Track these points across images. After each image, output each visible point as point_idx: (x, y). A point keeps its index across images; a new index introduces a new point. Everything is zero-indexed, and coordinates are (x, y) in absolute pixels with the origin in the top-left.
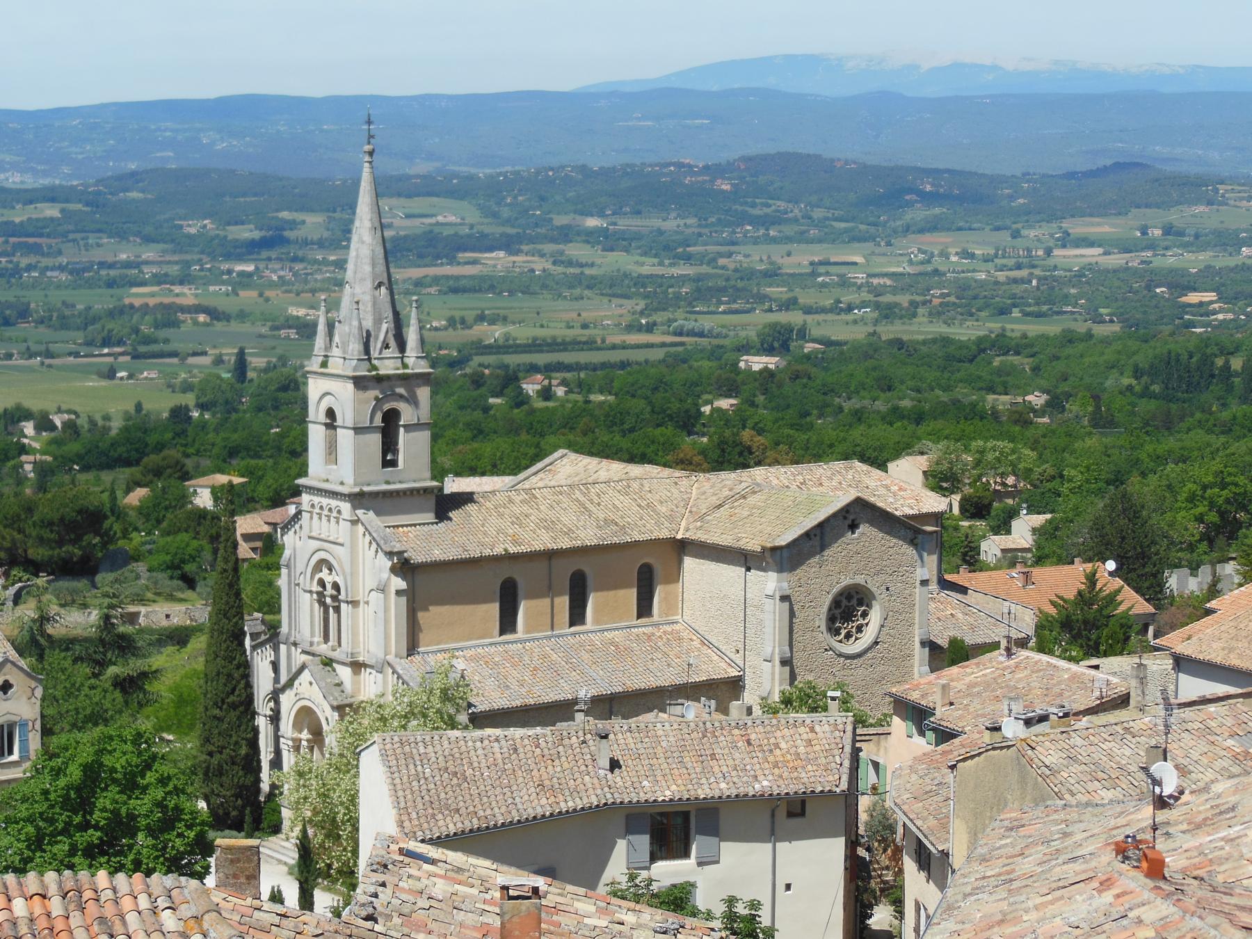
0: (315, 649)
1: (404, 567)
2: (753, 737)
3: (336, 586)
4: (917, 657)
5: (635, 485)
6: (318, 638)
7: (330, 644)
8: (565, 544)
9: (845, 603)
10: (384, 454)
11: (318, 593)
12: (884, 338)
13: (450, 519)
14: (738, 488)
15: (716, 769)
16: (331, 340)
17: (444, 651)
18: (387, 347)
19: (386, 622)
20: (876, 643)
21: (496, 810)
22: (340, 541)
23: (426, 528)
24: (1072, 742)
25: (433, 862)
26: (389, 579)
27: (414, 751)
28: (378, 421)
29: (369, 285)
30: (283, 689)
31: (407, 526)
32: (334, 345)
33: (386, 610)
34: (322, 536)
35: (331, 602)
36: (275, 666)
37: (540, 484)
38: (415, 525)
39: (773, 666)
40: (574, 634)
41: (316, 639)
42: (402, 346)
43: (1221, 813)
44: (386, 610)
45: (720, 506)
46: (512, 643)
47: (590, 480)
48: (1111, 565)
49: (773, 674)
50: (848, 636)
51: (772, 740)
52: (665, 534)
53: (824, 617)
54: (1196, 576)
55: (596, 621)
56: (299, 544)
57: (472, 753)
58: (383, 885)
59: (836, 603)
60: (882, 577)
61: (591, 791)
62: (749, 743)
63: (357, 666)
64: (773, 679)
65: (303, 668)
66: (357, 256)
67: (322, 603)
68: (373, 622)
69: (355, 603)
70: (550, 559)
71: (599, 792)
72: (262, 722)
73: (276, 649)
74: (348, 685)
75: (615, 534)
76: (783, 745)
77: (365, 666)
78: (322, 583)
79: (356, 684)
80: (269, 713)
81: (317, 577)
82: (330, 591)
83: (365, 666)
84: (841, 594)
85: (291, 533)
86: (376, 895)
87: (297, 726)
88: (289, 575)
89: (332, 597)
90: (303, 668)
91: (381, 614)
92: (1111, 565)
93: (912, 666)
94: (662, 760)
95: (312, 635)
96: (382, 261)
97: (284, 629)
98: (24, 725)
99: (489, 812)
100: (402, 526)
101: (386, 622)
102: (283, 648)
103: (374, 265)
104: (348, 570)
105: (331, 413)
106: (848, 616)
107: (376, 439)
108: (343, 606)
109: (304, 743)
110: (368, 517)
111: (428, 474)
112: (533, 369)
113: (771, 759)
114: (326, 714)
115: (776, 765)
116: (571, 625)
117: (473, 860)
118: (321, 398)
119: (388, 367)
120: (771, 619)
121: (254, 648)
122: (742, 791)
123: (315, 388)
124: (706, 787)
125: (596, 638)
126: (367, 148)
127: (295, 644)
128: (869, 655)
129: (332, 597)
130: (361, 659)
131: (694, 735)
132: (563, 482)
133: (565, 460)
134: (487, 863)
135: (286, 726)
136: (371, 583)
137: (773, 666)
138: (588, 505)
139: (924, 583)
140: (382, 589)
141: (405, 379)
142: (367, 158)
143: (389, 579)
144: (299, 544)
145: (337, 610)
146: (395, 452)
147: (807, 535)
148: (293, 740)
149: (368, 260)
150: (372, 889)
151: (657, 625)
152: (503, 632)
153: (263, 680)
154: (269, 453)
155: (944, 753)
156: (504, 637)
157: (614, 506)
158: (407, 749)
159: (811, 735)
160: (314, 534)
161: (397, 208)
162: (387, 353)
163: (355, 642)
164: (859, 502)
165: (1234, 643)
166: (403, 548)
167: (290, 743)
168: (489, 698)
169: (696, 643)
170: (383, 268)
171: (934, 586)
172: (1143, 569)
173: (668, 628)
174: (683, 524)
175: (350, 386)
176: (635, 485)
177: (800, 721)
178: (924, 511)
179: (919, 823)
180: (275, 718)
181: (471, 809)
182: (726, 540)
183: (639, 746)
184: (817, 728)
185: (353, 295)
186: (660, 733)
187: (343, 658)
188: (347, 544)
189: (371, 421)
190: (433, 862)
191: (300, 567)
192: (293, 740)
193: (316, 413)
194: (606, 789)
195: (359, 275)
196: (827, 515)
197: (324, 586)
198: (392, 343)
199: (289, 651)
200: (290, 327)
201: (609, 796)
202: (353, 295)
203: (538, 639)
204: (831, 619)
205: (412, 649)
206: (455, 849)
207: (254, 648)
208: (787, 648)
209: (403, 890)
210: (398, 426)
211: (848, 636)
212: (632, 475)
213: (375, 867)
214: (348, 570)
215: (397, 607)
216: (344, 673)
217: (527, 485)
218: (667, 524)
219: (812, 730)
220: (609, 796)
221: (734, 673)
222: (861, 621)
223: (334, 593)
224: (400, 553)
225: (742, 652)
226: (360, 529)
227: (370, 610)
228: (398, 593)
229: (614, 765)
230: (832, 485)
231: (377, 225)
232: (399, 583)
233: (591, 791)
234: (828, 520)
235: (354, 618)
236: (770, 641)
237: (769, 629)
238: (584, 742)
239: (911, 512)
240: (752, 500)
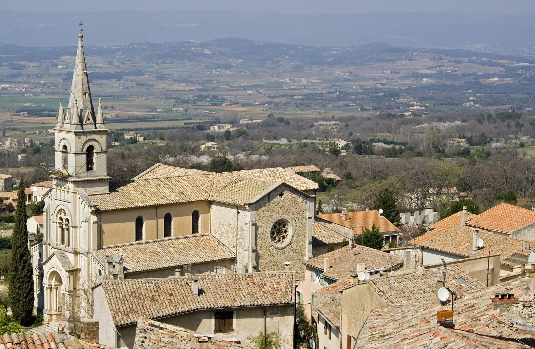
0: (58, 247)
1: (97, 212)
2: (255, 281)
3: (67, 220)
4: (307, 249)
5: (191, 178)
6: (59, 242)
7: (65, 245)
8: (162, 202)
9: (278, 226)
11: (60, 223)
12: (276, 117)
13: (118, 191)
14: (233, 179)
15: (241, 294)
16: (65, 117)
18: (89, 119)
19: (89, 235)
20: (291, 243)
21: (153, 312)
22: (69, 201)
23: (105, 196)
24: (391, 282)
25: (162, 329)
26: (90, 217)
27: (118, 288)
28: (85, 150)
29: (81, 93)
30: (44, 264)
31: (97, 195)
32: (66, 118)
33: (89, 230)
34: (61, 199)
35: (65, 228)
36: (41, 255)
37: (150, 177)
38: (100, 194)
39: (249, 253)
41: (58, 243)
42: (95, 120)
43: (469, 307)
44: (89, 230)
45: (226, 187)
46: (141, 244)
47: (171, 176)
48: (381, 211)
49: (249, 256)
50: (279, 240)
51: (263, 282)
52: (203, 198)
53: (269, 232)
54: (413, 216)
56: (51, 202)
57: (141, 288)
58: (145, 338)
59: (274, 227)
60: (292, 216)
61: (191, 303)
62: (254, 283)
63: (76, 253)
64: (249, 259)
65: (53, 254)
66: (76, 81)
67: (61, 227)
68: (83, 235)
69: (75, 227)
70: (156, 208)
71: (194, 304)
72: (35, 279)
73: (41, 246)
74: (72, 262)
75: (183, 198)
76: (268, 284)
77: (80, 253)
78: (61, 219)
79: (76, 261)
80: (38, 274)
81: (59, 216)
82: (64, 222)
83: (80, 253)
84: (276, 223)
85: (47, 197)
86: (143, 342)
87: (50, 278)
88: (47, 216)
89: (66, 225)
90: (53, 254)
91: (87, 232)
92: (381, 211)
93: (305, 253)
94: (219, 291)
95: (57, 241)
96: (86, 83)
97: (45, 239)
99: (150, 312)
100: (95, 195)
101: (89, 235)
102: (44, 246)
104: (72, 214)
105: (65, 147)
106: (279, 232)
107: (83, 158)
108: (71, 228)
109: (53, 286)
110: (80, 189)
111: (106, 174)
112: (130, 130)
113: (263, 290)
114: (64, 275)
115: (265, 292)
116: (165, 237)
117: (177, 328)
118: (60, 141)
119: (89, 128)
120: (248, 233)
121: (31, 246)
122: (252, 303)
123: (58, 136)
124: (237, 301)
125: (175, 242)
126: (80, 35)
127: (49, 245)
128: (288, 248)
129: (66, 225)
130: (78, 251)
131: (232, 280)
132: (160, 177)
133: (160, 168)
134: (183, 329)
135: (46, 280)
136: (82, 219)
137: (249, 253)
138: (172, 186)
139: (310, 218)
140: (87, 221)
142: (80, 39)
143: (90, 217)
144: (51, 202)
145: (68, 230)
146: (92, 164)
147: (263, 198)
148: (49, 285)
149: (80, 83)
150: (142, 339)
151: (200, 236)
152: (137, 239)
153: (35, 262)
155: (333, 287)
156: (138, 242)
157: (182, 186)
158: (115, 287)
159: (279, 280)
160: (57, 198)
161: (94, 61)
162: (88, 122)
163: (75, 244)
165: (445, 242)
166: (96, 204)
167: (48, 287)
168: (133, 267)
169: (217, 244)
170: (86, 86)
171: (313, 220)
172: (392, 213)
173: (205, 238)
174: (211, 194)
175: (73, 135)
176: (191, 178)
177: (274, 275)
178: (309, 188)
179: (327, 316)
180: (41, 276)
181: (143, 311)
182: (229, 201)
183: (209, 285)
184: (281, 277)
185: (74, 98)
186: (217, 279)
187: (70, 250)
188: (72, 202)
189: (82, 151)
190: (162, 329)
191: (52, 212)
192: (49, 285)
193: (58, 146)
194: (197, 303)
195: (77, 89)
196: (271, 190)
197: (62, 220)
198: (91, 118)
199: (46, 247)
200: (23, 111)
201: (198, 305)
202: (74, 98)
203: (151, 242)
205: (100, 247)
206: (169, 323)
207: (31, 246)
208: (254, 246)
209: (152, 339)
210: (93, 153)
211: (279, 240)
212: (188, 173)
213: (141, 331)
214: (72, 214)
215: (93, 229)
216: (71, 257)
217: (144, 178)
218: (204, 194)
219: (279, 278)
220: (198, 305)
221: (232, 256)
222: (284, 234)
223: (67, 223)
224: (95, 206)
225: (236, 247)
226: (78, 196)
227: (82, 230)
228: (94, 223)
229: (201, 292)
230: (269, 178)
231: (84, 68)
232: (94, 218)
233: (191, 303)
234: (271, 192)
235: (75, 233)
236: (248, 242)
237: (247, 238)
238: (187, 283)
239: (304, 189)
240: (239, 184)
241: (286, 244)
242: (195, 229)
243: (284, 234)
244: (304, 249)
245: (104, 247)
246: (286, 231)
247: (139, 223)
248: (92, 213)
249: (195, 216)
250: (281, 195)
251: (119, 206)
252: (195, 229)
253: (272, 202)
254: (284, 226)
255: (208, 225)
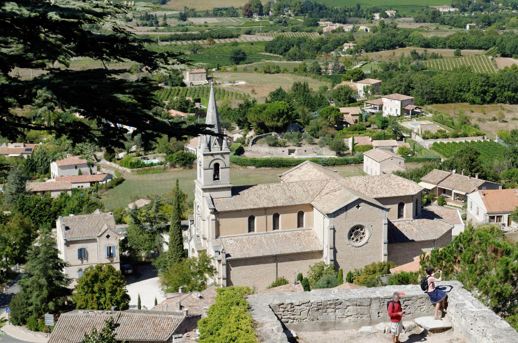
1: (214, 211)
10: (214, 176)
17: (229, 237)
20: (367, 243)
28: (212, 166)
40: (274, 233)
50: (357, 240)
55: (282, 228)
98: (114, 247)
103: (212, 119)
107: (211, 172)
141: (222, 154)
149: (211, 118)
151: (304, 230)
154: (441, 46)
162: (215, 146)
164: (359, 199)
204: (350, 235)
205: (217, 236)
222: (362, 236)
228: (212, 220)
232: (213, 217)
241: (363, 243)
242: (300, 224)
243: (362, 236)
244: (381, 247)
245: (221, 236)
246: (363, 234)
247: (251, 219)
248: (211, 213)
249: (301, 215)
250: (358, 207)
251: (234, 208)
252: (300, 224)
253: (348, 211)
254: (362, 230)
255: (311, 223)
